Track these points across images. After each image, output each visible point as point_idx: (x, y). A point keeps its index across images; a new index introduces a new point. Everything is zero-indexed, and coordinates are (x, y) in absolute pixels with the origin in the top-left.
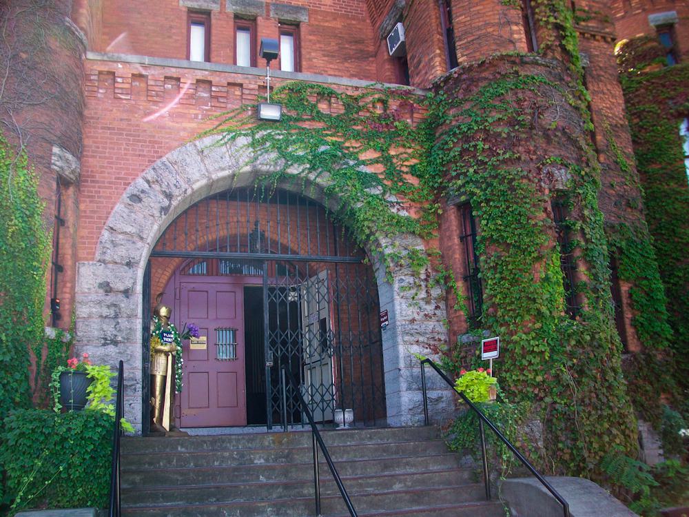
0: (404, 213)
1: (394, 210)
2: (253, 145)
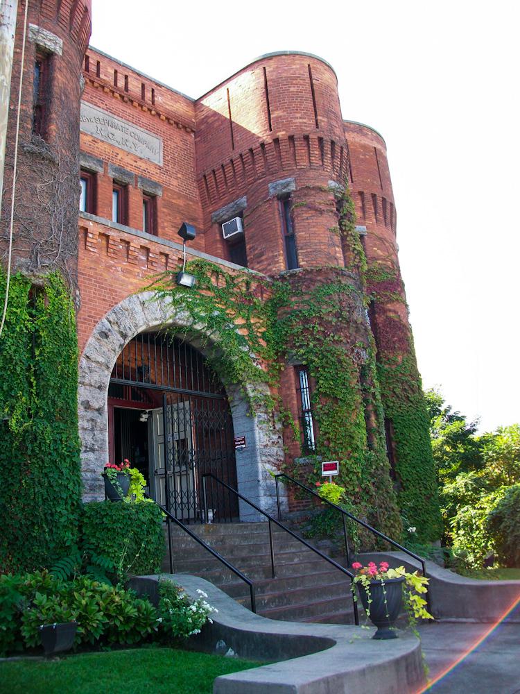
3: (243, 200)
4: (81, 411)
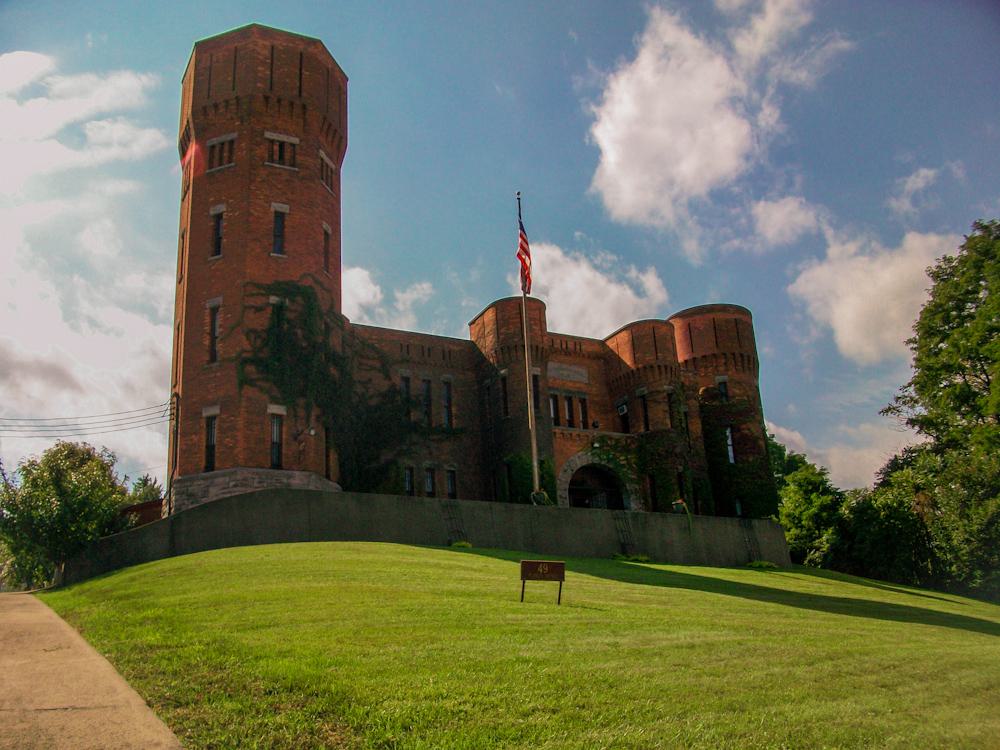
3: (626, 397)
4: (559, 498)
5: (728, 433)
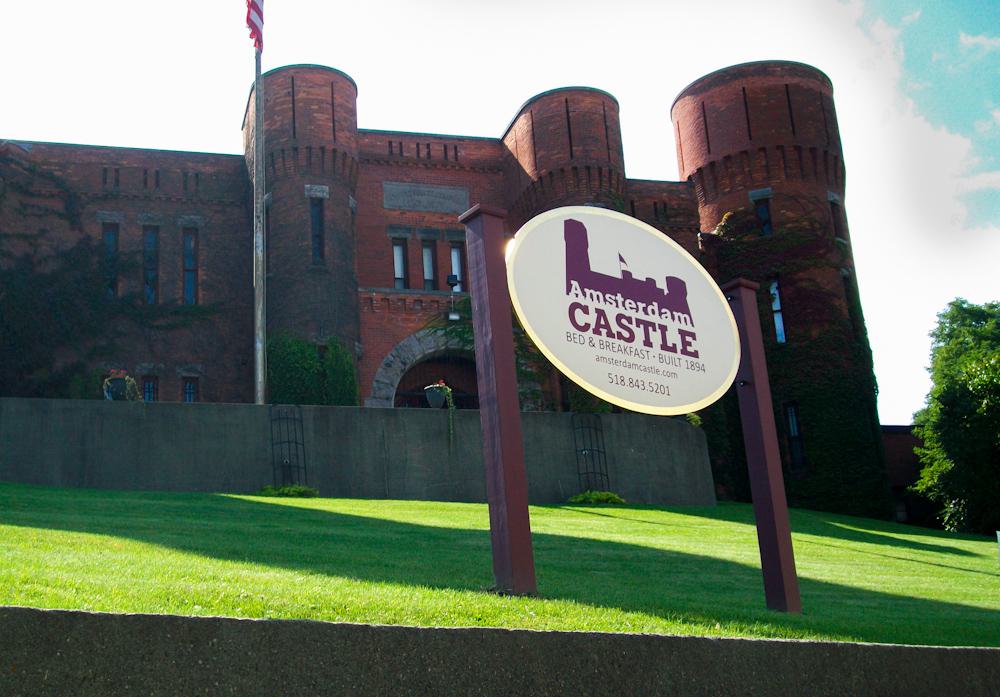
0: (529, 369)
1: (523, 368)
2: (445, 335)
5: (774, 290)
